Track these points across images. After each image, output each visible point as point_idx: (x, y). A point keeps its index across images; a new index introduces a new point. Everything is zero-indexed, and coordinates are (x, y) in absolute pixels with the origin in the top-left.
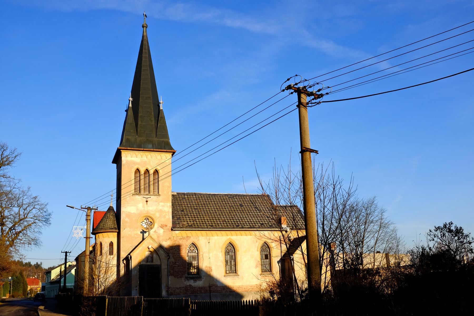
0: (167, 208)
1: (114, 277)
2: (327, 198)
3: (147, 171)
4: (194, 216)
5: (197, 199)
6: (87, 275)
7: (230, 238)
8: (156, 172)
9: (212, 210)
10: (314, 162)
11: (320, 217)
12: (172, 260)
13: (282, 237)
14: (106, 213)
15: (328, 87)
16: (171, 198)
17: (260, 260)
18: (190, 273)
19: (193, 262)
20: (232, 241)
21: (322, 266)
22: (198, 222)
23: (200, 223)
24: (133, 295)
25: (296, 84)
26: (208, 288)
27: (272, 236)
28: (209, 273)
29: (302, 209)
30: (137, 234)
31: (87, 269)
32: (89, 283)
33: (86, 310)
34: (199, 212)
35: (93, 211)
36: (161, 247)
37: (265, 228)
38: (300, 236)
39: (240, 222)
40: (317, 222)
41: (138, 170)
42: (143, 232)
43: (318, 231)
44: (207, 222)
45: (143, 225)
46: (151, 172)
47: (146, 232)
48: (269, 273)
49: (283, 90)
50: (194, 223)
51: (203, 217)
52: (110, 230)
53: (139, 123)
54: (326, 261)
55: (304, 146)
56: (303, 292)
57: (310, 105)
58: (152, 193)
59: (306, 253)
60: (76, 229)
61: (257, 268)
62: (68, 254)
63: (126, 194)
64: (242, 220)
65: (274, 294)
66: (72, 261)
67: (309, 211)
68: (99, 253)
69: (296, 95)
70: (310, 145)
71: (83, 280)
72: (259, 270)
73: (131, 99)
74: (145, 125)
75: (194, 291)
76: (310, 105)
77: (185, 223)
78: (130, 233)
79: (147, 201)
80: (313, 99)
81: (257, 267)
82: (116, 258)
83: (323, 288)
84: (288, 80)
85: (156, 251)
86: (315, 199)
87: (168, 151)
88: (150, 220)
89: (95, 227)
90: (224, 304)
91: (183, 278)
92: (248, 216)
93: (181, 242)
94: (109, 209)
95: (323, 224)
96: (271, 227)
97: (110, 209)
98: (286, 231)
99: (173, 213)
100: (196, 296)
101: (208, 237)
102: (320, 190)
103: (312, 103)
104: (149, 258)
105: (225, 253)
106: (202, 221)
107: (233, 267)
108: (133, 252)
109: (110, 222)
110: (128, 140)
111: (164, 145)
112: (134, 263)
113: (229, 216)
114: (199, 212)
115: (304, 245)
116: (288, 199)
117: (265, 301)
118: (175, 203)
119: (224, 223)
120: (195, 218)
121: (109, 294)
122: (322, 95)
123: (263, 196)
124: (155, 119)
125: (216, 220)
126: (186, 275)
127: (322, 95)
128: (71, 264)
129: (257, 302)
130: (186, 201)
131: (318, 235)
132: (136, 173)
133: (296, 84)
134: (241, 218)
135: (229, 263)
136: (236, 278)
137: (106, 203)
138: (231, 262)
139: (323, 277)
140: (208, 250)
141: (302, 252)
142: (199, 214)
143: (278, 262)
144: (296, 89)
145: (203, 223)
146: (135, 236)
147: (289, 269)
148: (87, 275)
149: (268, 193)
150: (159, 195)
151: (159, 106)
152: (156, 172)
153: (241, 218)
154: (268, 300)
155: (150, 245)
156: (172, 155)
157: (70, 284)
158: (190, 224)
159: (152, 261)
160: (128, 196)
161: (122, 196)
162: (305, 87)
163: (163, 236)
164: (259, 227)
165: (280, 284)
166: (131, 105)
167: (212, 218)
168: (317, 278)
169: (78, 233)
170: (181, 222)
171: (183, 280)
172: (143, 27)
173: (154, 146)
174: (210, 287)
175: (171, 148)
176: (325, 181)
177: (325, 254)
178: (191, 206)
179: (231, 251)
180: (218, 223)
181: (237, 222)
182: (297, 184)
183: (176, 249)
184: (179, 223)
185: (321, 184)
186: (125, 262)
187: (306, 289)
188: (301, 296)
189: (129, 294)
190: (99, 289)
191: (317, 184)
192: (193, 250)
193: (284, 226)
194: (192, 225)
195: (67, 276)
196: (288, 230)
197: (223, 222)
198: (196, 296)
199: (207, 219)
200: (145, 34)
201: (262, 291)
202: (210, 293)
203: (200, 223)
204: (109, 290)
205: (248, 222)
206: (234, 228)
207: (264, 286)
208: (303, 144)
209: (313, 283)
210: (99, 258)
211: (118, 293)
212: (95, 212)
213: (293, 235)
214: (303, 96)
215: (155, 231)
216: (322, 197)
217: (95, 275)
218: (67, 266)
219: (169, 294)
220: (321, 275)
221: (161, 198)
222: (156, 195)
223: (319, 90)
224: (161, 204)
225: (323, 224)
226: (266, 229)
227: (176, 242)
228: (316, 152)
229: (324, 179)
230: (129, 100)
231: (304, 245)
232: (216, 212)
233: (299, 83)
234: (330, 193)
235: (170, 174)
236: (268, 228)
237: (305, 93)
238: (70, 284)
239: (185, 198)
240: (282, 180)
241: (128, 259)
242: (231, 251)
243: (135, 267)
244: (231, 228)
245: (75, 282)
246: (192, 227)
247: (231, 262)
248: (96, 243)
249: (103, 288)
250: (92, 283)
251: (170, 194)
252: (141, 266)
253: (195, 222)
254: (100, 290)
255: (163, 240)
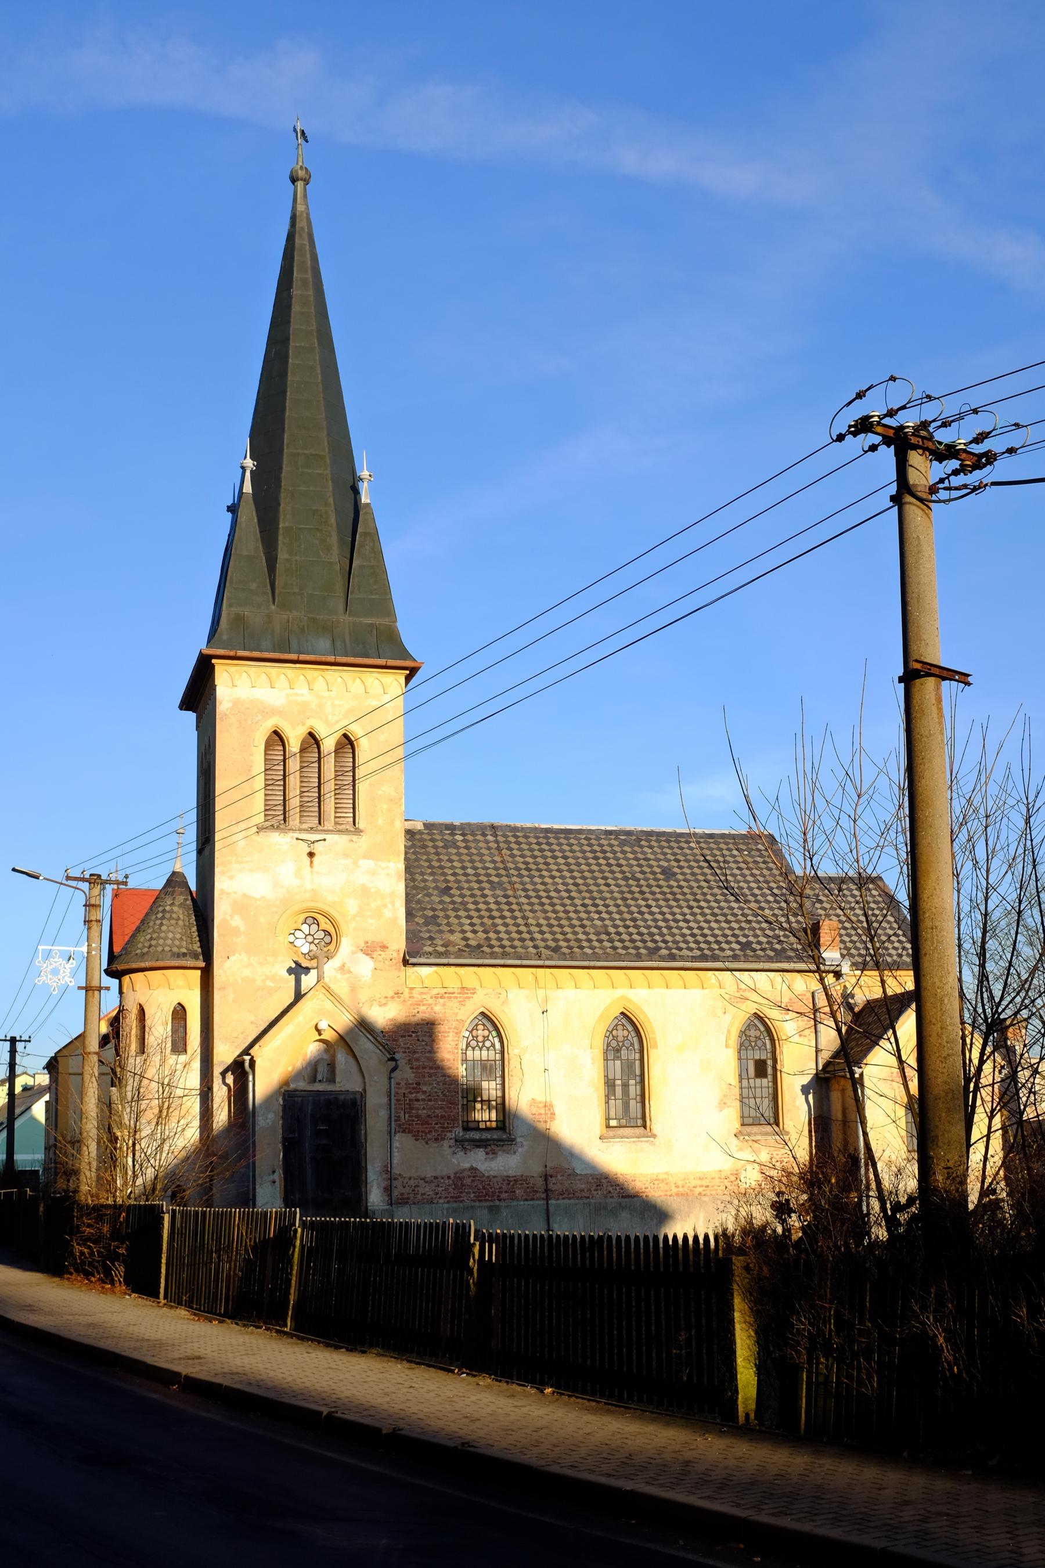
0: (389, 880)
1: (192, 1134)
2: (1001, 855)
3: (312, 739)
4: (489, 910)
5: (498, 849)
6: (91, 1128)
7: (624, 998)
8: (347, 743)
9: (557, 891)
10: (953, 718)
11: (971, 929)
12: (406, 1073)
13: (822, 1001)
14: (159, 897)
15: (1017, 425)
16: (400, 843)
17: (734, 1080)
18: (470, 1126)
19: (485, 1085)
20: (631, 1007)
21: (973, 1112)
22: (503, 935)
23: (511, 940)
24: (260, 1201)
25: (891, 413)
26: (540, 1182)
27: (779, 990)
28: (542, 1126)
29: (903, 897)
30: (273, 978)
31: (91, 1105)
32: (99, 1156)
33: (92, 1254)
34: (506, 896)
35: (109, 889)
36: (363, 1025)
37: (758, 958)
38: (890, 993)
39: (662, 935)
40: (960, 946)
41: (277, 737)
42: (298, 970)
43: (960, 980)
44: (538, 936)
45: (298, 943)
46: (328, 745)
47: (307, 970)
48: (769, 1129)
49: (841, 438)
50: (488, 939)
51: (524, 918)
52: (175, 963)
53: (282, 555)
54: (986, 1098)
55: (914, 655)
56: (898, 1207)
57: (943, 495)
58: (329, 824)
59: (912, 1061)
60: (48, 955)
61: (726, 1111)
62: (19, 1046)
63: (235, 829)
64: (669, 928)
65: (790, 1211)
66: (33, 1073)
67: (928, 903)
68: (134, 1046)
69: (887, 455)
70: (939, 651)
71: (77, 1142)
72: (731, 1117)
73: (249, 463)
74: (302, 564)
75: (489, 1192)
76: (943, 495)
77: (456, 937)
78: (247, 972)
79: (311, 855)
80: (956, 472)
81: (723, 1104)
82: (196, 1065)
83: (973, 1199)
84: (860, 395)
85: (344, 1041)
86: (953, 857)
87: (391, 662)
88: (325, 924)
89: (117, 950)
90: (596, 1243)
91: (446, 1144)
92: (694, 914)
93: (437, 1010)
94: (169, 882)
95: (982, 954)
96: (780, 955)
97: (175, 881)
98: (838, 975)
99: (409, 898)
100: (494, 1210)
101: (541, 993)
102: (975, 825)
103: (949, 489)
104: (321, 1068)
105: (605, 1053)
106: (520, 932)
107: (632, 1103)
108: (261, 1042)
109: (176, 929)
110: (239, 621)
111: (372, 642)
112: (264, 1083)
113: (620, 913)
114: (506, 896)
115: (907, 1026)
116: (850, 859)
117: (755, 1235)
118: (417, 860)
119: (600, 941)
120: (492, 917)
121: (173, 1196)
122: (989, 458)
123: (751, 838)
124: (341, 540)
125: (572, 926)
126: (459, 1132)
127: (989, 458)
128: (30, 1082)
129: (724, 1236)
130: (458, 854)
131: (962, 995)
132: (268, 746)
133: (891, 413)
134: (666, 920)
135: (619, 1090)
136: (644, 1145)
137: (160, 859)
138: (625, 1086)
139: (976, 1156)
140: (543, 1043)
141: (899, 1058)
142: (509, 904)
143: (805, 1090)
144: (891, 433)
145: (522, 940)
146: (269, 983)
147: (844, 1111)
148: (91, 1128)
149: (772, 829)
150: (358, 832)
151: (356, 492)
152: (347, 743)
153: (666, 920)
154: (763, 1228)
155: (320, 1019)
156: (408, 679)
157: (29, 1157)
158: (473, 943)
159: (332, 1080)
160: (241, 835)
161: (218, 836)
162: (924, 425)
163: (371, 985)
164: (735, 958)
165: (811, 1178)
166: (248, 488)
167: (558, 919)
168: (953, 1157)
169: (55, 972)
170: (441, 932)
171: (447, 1151)
172: (294, 180)
173: (338, 644)
174: (546, 1177)
175: (405, 654)
176: (993, 789)
177: (988, 1067)
178: (477, 875)
179: (627, 1045)
180: (578, 940)
181: (651, 935)
182: (887, 803)
183: (417, 1037)
184: (431, 938)
185: (977, 801)
186: (230, 1079)
187: (911, 1200)
188: (891, 1223)
189: (247, 1199)
190: (135, 1176)
191: (963, 801)
192: (486, 1038)
193: (831, 955)
194: (479, 946)
195: (18, 1124)
196: (846, 968)
197: (597, 934)
198: (494, 1210)
199: (539, 925)
200: (300, 208)
201: (744, 1196)
202: (547, 1199)
203: (511, 940)
204: (172, 1184)
205: (693, 935)
206: (639, 957)
207: (752, 1177)
208: (913, 647)
209: (940, 1178)
210: (134, 1062)
211: (206, 1195)
212: (116, 895)
213: (867, 988)
214: (915, 458)
215: (342, 968)
216: (981, 854)
217: (121, 1125)
218: (18, 1089)
219: (393, 1200)
220: (969, 1145)
221: (363, 842)
222: (346, 832)
223: (980, 439)
224: (366, 864)
225: (982, 954)
226: (761, 966)
227: (422, 1008)
228: (963, 678)
229: (991, 783)
230: (243, 468)
231: (907, 1026)
232: (571, 898)
233: (903, 408)
234: (1014, 836)
235: (400, 752)
236: (770, 959)
237: (925, 449)
238: (30, 1156)
239: (454, 844)
240: (829, 782)
241: (241, 1070)
242: (627, 1045)
243: (269, 1099)
244: (628, 957)
245: (47, 1148)
246: (480, 953)
247: (625, 1086)
248: (121, 1010)
249: (150, 1173)
250: (110, 1159)
251: (399, 827)
252: (291, 1099)
253: (492, 935)
254: (139, 1181)
255: (371, 1001)
